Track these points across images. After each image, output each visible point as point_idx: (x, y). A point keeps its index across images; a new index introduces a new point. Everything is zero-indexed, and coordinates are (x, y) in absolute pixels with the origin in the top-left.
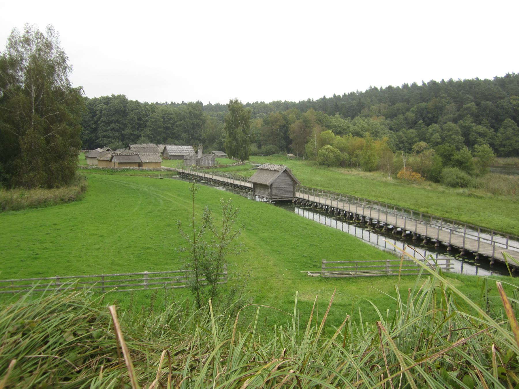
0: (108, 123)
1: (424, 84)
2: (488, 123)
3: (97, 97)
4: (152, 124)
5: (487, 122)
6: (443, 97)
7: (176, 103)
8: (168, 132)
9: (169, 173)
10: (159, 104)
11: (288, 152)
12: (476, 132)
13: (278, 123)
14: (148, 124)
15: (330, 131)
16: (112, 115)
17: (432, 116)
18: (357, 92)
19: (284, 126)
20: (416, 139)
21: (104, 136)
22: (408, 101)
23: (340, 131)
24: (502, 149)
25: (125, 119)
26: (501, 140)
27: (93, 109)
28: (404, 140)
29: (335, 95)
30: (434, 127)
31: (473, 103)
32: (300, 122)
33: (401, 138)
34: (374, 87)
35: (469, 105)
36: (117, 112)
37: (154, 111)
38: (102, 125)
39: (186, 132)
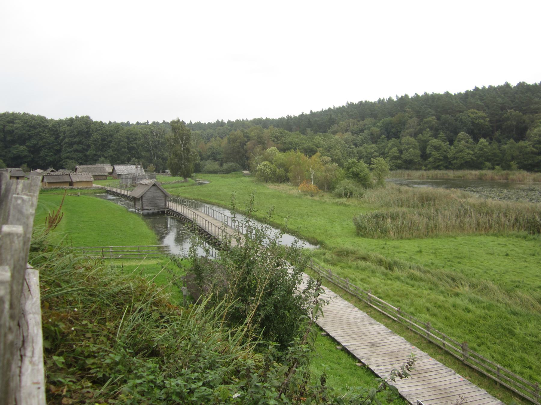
0: (71, 144)
1: (455, 94)
2: (445, 137)
3: (62, 119)
4: (116, 144)
5: (444, 135)
7: (292, 116)
8: (134, 152)
9: (98, 191)
10: (141, 124)
11: (245, 169)
12: (432, 146)
13: (239, 141)
14: (112, 144)
16: (75, 136)
18: (334, 108)
20: (376, 154)
21: (67, 158)
24: (455, 161)
25: (88, 140)
26: (454, 152)
27: (57, 131)
28: (364, 155)
31: (434, 117)
33: (362, 152)
35: (430, 118)
36: (80, 133)
38: (66, 147)
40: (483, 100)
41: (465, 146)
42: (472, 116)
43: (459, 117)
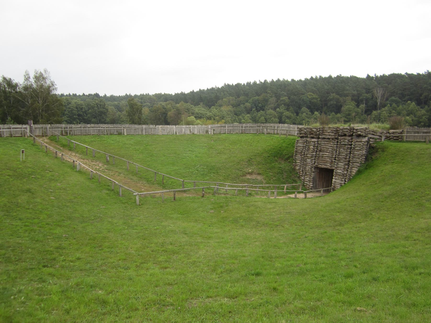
4: (69, 112)
6: (268, 93)
12: (285, 116)
15: (193, 117)
17: (262, 106)
18: (216, 87)
19: (164, 113)
22: (247, 95)
23: (201, 116)
29: (200, 89)
30: (261, 113)
32: (174, 111)
34: (228, 84)
35: (284, 98)
37: (70, 104)
39: (94, 118)
41: (306, 116)
43: (302, 97)
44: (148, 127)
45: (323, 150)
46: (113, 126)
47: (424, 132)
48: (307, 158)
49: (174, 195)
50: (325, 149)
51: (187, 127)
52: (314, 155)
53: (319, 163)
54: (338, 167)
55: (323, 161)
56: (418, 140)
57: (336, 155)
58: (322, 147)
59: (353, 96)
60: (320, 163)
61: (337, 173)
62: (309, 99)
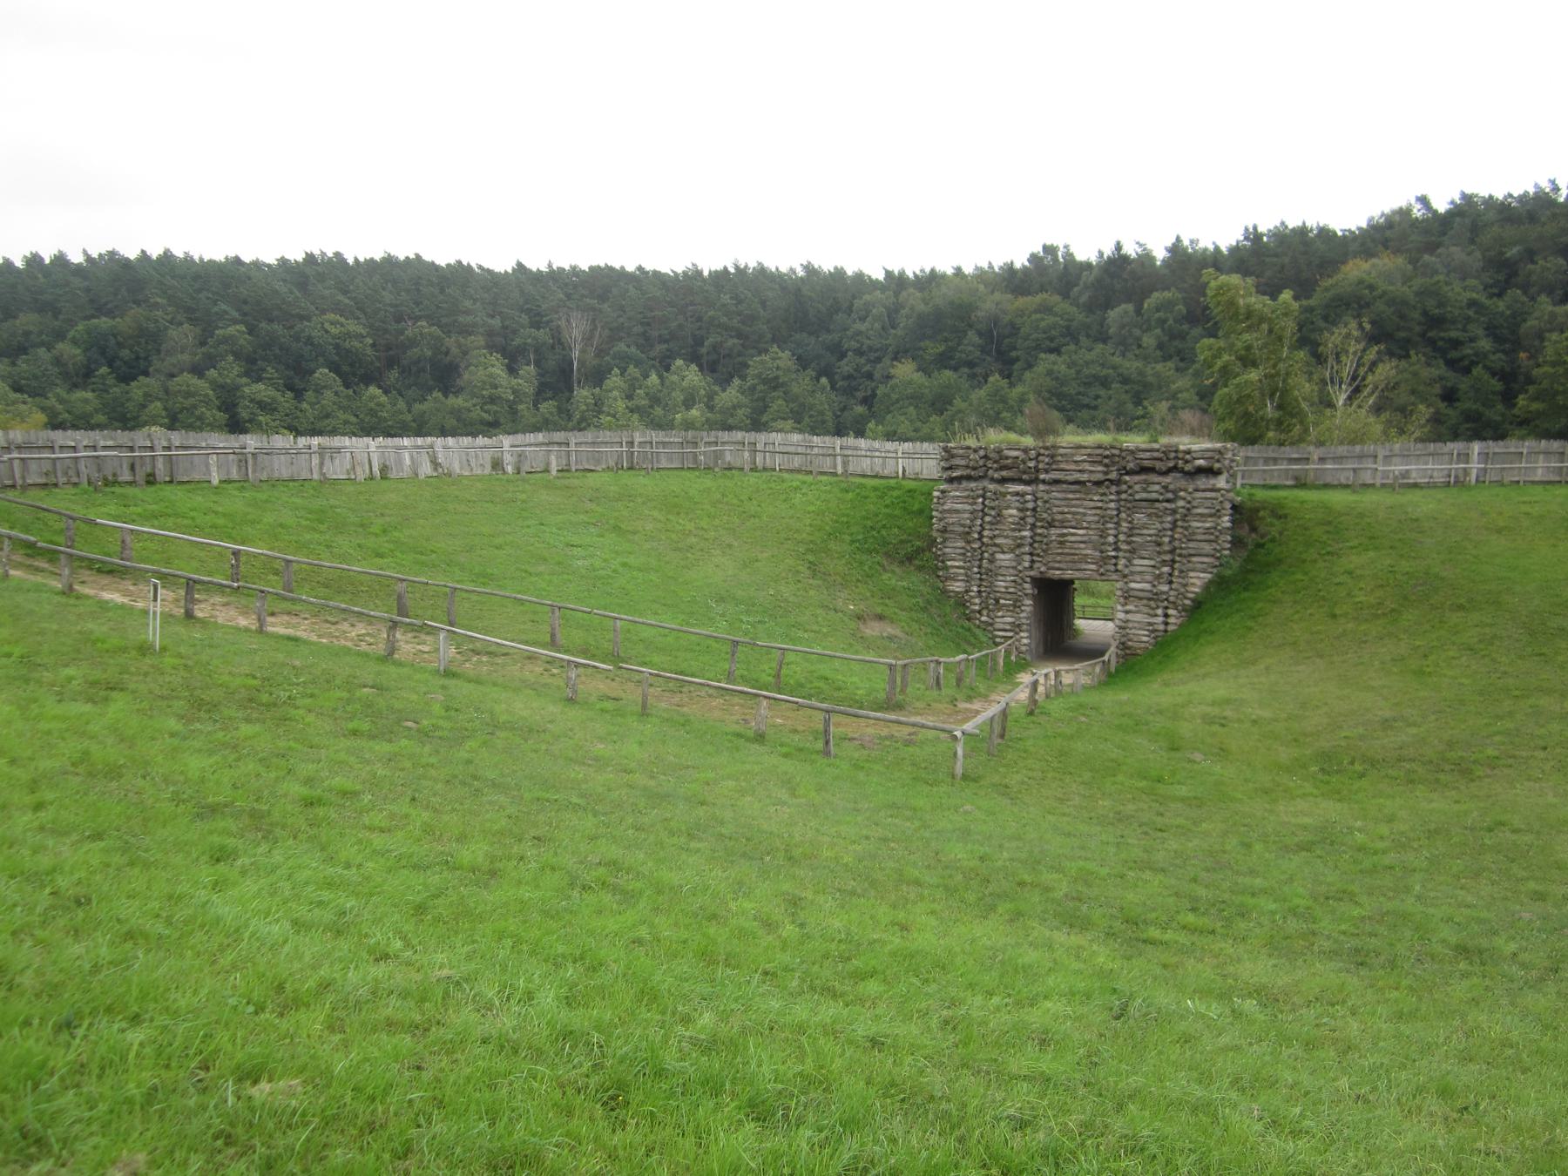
5: (276, 375)
12: (252, 401)
17: (133, 356)
22: (48, 308)
35: (231, 330)
40: (348, 292)
41: (334, 403)
42: (334, 330)
43: (303, 331)
44: (266, 445)
45: (1062, 521)
46: (112, 439)
47: (1291, 461)
48: (994, 549)
49: (827, 723)
50: (1069, 516)
51: (419, 447)
52: (1025, 537)
53: (1051, 564)
54: (1132, 573)
55: (1069, 558)
56: (1274, 482)
57: (1116, 536)
58: (1055, 510)
59: (490, 334)
60: (1057, 565)
61: (1131, 593)
62: (333, 338)
